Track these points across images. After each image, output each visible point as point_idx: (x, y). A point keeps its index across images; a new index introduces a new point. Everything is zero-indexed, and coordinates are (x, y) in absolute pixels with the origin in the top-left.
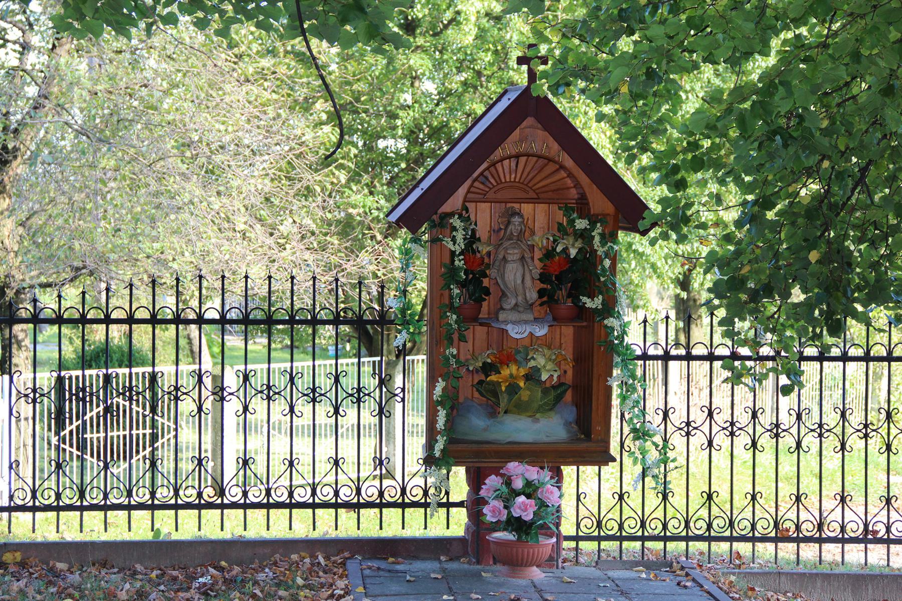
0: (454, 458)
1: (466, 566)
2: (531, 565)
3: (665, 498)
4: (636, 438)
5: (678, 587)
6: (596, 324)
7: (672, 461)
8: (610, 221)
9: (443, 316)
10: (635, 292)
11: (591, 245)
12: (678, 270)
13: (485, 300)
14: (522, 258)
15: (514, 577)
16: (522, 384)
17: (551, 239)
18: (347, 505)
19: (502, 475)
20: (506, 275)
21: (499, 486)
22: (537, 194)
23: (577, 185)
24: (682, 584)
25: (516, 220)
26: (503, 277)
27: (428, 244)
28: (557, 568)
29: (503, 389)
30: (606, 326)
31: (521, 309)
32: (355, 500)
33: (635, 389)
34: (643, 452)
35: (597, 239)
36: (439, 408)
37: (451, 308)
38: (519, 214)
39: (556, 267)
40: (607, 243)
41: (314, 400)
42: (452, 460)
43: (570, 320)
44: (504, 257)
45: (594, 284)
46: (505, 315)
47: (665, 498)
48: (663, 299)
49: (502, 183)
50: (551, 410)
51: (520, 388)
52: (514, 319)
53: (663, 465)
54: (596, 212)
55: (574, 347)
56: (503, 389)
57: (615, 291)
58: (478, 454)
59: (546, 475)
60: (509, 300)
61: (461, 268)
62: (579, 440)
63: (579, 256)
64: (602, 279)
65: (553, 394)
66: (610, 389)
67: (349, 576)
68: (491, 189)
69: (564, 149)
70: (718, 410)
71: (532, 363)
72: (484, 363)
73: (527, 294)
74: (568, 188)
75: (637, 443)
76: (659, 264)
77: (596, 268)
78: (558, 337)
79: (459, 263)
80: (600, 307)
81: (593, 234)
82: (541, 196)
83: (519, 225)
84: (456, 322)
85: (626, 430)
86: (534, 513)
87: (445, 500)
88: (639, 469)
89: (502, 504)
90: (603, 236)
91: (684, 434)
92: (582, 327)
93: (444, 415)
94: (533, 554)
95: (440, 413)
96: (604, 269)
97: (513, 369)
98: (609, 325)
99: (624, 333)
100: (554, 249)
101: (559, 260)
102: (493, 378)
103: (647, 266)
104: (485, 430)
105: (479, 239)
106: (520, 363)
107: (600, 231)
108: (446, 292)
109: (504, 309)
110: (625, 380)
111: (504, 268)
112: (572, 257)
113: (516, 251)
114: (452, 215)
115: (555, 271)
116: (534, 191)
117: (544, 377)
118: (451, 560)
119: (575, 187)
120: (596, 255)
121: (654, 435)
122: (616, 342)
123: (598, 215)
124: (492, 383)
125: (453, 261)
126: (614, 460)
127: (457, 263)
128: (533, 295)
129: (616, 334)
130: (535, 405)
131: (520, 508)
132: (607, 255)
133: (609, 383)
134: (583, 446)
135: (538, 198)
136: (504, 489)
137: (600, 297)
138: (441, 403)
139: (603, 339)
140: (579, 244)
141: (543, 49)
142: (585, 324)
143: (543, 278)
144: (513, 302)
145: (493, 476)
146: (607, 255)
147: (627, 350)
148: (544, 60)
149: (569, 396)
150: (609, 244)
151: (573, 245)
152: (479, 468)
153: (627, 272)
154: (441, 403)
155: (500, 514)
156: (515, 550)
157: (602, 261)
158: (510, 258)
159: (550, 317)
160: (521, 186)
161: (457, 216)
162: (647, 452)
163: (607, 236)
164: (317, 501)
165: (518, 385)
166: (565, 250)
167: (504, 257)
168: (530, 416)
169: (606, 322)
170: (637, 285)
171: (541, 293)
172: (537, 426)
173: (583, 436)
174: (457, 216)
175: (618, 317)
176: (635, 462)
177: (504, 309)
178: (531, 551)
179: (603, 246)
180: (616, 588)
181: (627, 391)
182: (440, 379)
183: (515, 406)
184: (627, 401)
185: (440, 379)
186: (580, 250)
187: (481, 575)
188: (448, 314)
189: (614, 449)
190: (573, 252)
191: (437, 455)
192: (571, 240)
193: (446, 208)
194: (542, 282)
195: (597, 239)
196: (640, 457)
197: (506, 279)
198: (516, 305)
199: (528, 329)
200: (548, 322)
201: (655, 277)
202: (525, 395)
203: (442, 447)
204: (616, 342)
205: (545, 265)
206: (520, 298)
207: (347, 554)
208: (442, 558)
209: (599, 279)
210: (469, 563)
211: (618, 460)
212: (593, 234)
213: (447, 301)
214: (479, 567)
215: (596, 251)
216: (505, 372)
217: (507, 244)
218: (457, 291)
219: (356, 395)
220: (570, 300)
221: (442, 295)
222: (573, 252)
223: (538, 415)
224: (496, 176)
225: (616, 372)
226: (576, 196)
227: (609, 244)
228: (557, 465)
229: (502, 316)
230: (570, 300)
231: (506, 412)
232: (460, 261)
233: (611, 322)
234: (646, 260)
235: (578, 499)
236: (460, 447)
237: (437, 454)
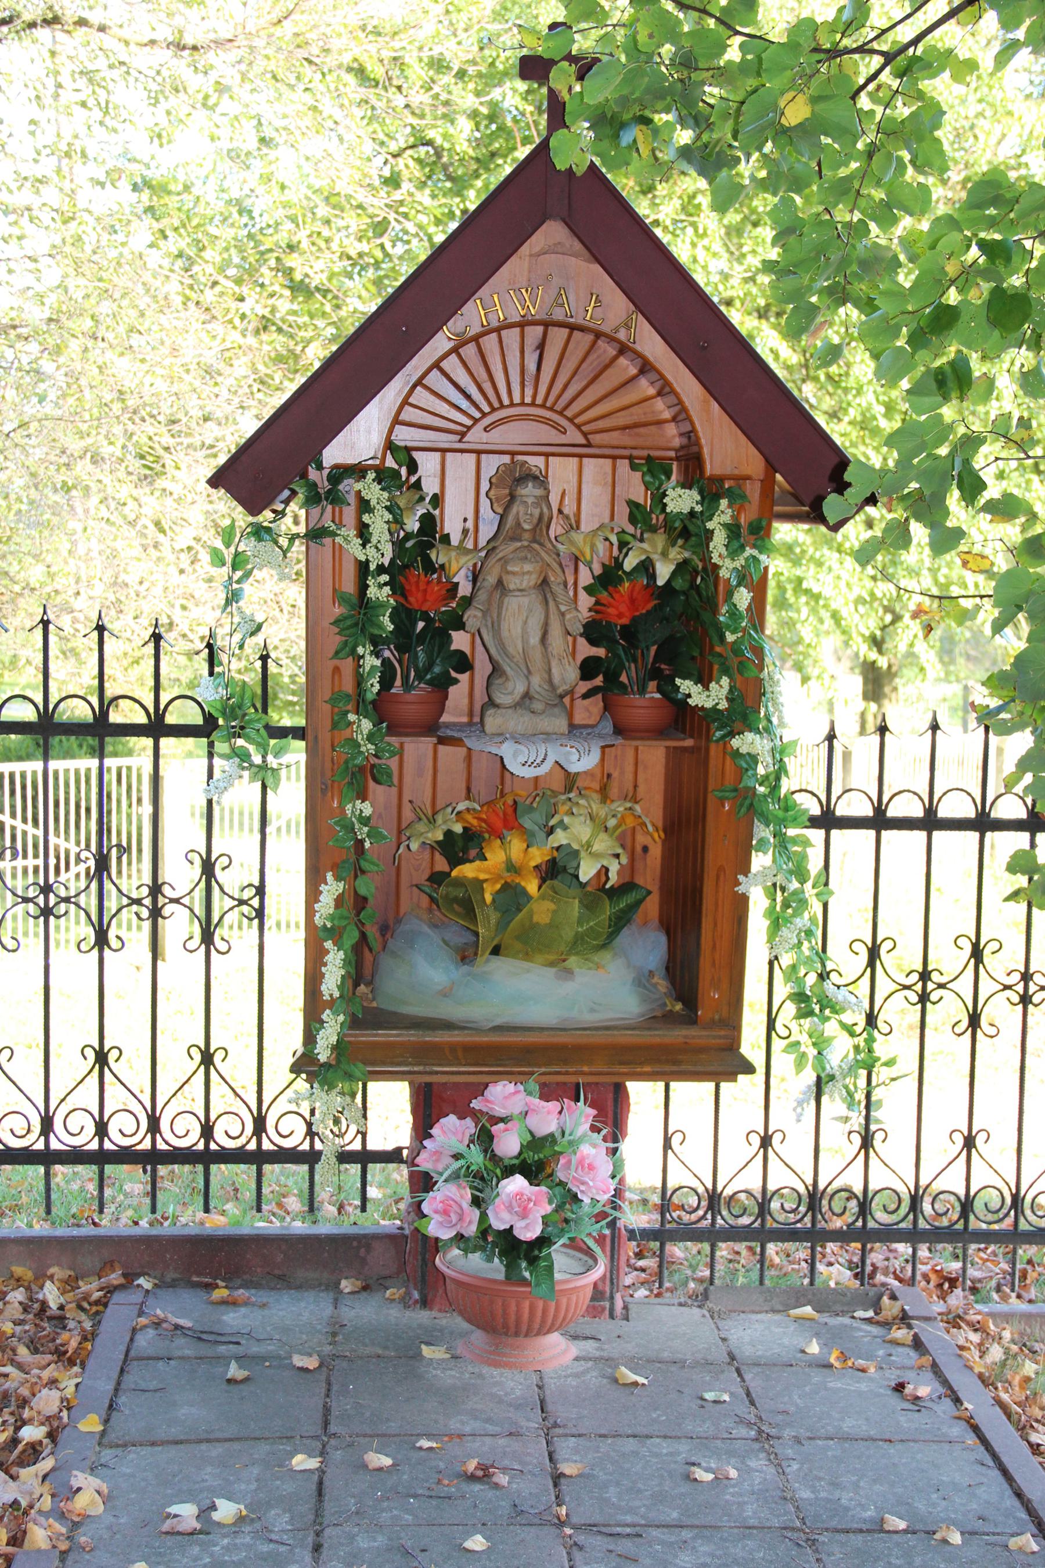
0: (366, 1063)
1: (395, 1313)
2: (545, 1329)
3: (867, 1143)
4: (805, 1013)
5: (894, 1401)
6: (713, 747)
7: (887, 1064)
8: (753, 491)
9: (338, 722)
10: (806, 655)
11: (706, 558)
12: (871, 624)
13: (456, 681)
14: (544, 584)
15: (496, 1364)
16: (532, 886)
17: (614, 539)
18: (126, 1156)
19: (475, 1115)
20: (504, 626)
21: (462, 1148)
22: (585, 435)
23: (681, 414)
24: (909, 1389)
25: (529, 491)
26: (496, 630)
27: (299, 549)
28: (612, 1316)
29: (488, 898)
30: (737, 753)
31: (538, 706)
32: (147, 1145)
33: (803, 903)
34: (821, 1043)
35: (720, 538)
36: (328, 944)
37: (360, 705)
38: (540, 480)
39: (623, 608)
40: (742, 548)
41: (46, 912)
42: (358, 1070)
43: (659, 733)
44: (500, 583)
45: (712, 647)
46: (499, 720)
47: (867, 1143)
48: (839, 659)
49: (502, 406)
50: (603, 946)
51: (529, 898)
52: (520, 729)
53: (863, 1073)
54: (718, 472)
55: (666, 791)
56: (488, 898)
57: (761, 667)
58: (424, 1053)
59: (582, 1115)
60: (510, 685)
61: (382, 605)
62: (668, 1018)
63: (679, 584)
64: (730, 638)
65: (608, 910)
66: (743, 901)
67: (91, 1364)
68: (476, 421)
69: (639, 309)
70: (995, 946)
71: (560, 838)
72: (449, 834)
73: (554, 671)
74: (660, 423)
75: (807, 1023)
76: (844, 613)
77: (715, 611)
78: (629, 768)
79: (378, 591)
80: (723, 705)
81: (710, 525)
82: (596, 439)
83: (537, 504)
84: (370, 738)
85: (782, 990)
86: (546, 1221)
87: (357, 1146)
88: (809, 1077)
89: (468, 1193)
90: (733, 531)
91: (914, 998)
92: (684, 749)
93: (339, 962)
94: (545, 1311)
95: (329, 958)
96: (734, 613)
97: (516, 846)
98: (743, 750)
99: (781, 771)
100: (619, 565)
101: (632, 590)
102: (468, 871)
103: (826, 615)
104: (445, 993)
105: (446, 539)
106: (532, 834)
107: (727, 518)
108: (347, 665)
109: (497, 706)
110: (779, 880)
111: (500, 607)
112: (660, 582)
113: (528, 567)
114: (358, 471)
115: (620, 615)
116: (578, 427)
117: (587, 871)
118: (365, 1288)
119: (660, 394)
120: (717, 577)
121: (843, 1010)
122: (761, 789)
123: (721, 479)
124: (460, 883)
125: (363, 587)
126: (750, 1069)
127: (372, 592)
128: (567, 674)
129: (761, 770)
130: (568, 934)
131: (509, 1208)
132: (743, 578)
133: (740, 889)
134: (677, 1035)
135: (589, 445)
136: (476, 1157)
137: (725, 681)
138: (335, 933)
139: (728, 785)
140: (677, 554)
141: (584, 43)
142: (689, 743)
143: (593, 632)
144: (520, 688)
145: (452, 1119)
146: (743, 578)
147: (786, 809)
148: (584, 67)
149: (652, 906)
150: (749, 551)
151: (664, 554)
152: (429, 1085)
153: (794, 625)
154: (335, 933)
155: (461, 1218)
156: (499, 1301)
157: (730, 593)
158: (512, 583)
159: (608, 727)
160: (548, 414)
161: (371, 475)
162: (828, 1041)
163: (744, 531)
164: (55, 1145)
165: (524, 892)
166: (646, 567)
167: (500, 583)
168: (552, 964)
169: (735, 742)
170: (809, 645)
171: (589, 668)
172: (569, 987)
173: (679, 1007)
174: (371, 475)
175: (767, 730)
176: (800, 1063)
177: (497, 706)
178: (540, 1304)
179: (733, 554)
180: (743, 1409)
181: (786, 905)
182: (329, 876)
183: (518, 938)
184: (784, 932)
185: (329, 876)
186: (682, 567)
187: (418, 1356)
188: (352, 717)
189: (751, 1045)
190: (663, 572)
191: (323, 1058)
192: (660, 540)
193: (334, 454)
194: (593, 642)
195: (720, 538)
196: (812, 1052)
197: (505, 634)
198: (527, 695)
199: (554, 753)
200: (601, 736)
201: (838, 632)
202: (541, 911)
203: (334, 1039)
204: (761, 789)
205: (597, 603)
206: (536, 680)
207: (115, 1278)
208: (344, 1283)
209: (722, 638)
210: (405, 1302)
211: (759, 1063)
212: (710, 525)
213: (348, 686)
214: (423, 1316)
215: (716, 567)
216: (496, 856)
217: (506, 549)
218: (371, 662)
219: (147, 902)
220: (652, 685)
221: (337, 670)
222: (663, 572)
223: (573, 961)
224: (487, 387)
225: (760, 861)
226: (677, 442)
227: (749, 551)
228: (616, 1079)
229: (493, 721)
230: (652, 685)
231: (496, 951)
232: (381, 586)
233: (746, 742)
234: (824, 606)
235: (667, 1145)
236: (382, 1036)
237: (323, 1054)
